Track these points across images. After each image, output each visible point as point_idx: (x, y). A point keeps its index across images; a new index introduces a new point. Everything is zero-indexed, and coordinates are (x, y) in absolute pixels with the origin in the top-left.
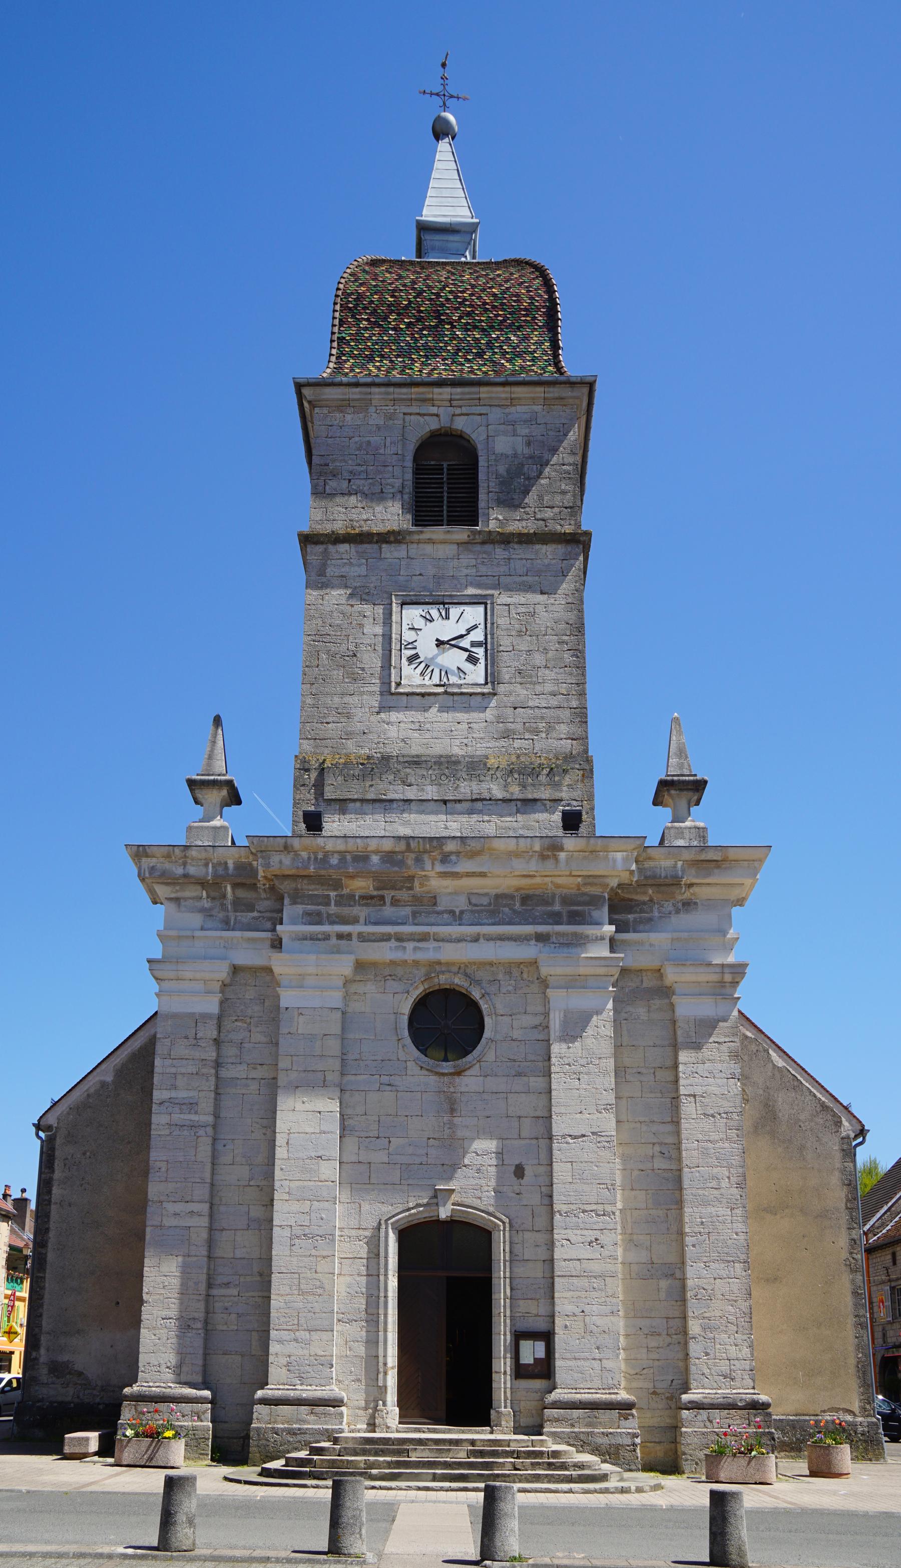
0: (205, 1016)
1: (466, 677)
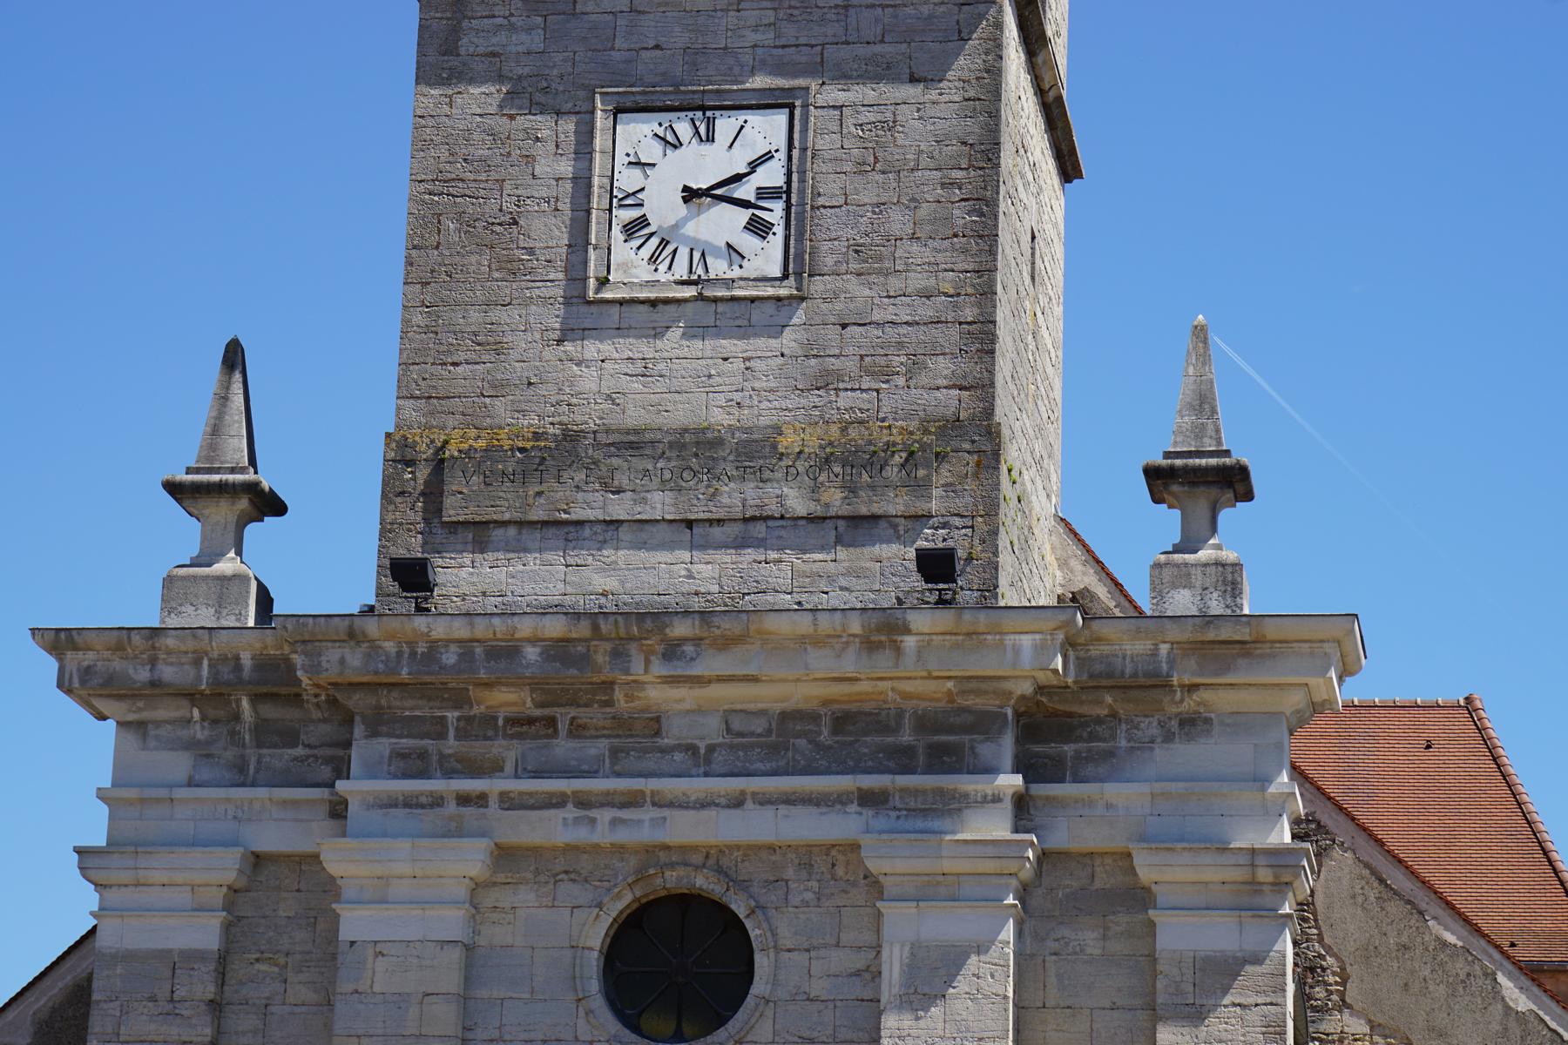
0: (192, 957)
1: (745, 263)
